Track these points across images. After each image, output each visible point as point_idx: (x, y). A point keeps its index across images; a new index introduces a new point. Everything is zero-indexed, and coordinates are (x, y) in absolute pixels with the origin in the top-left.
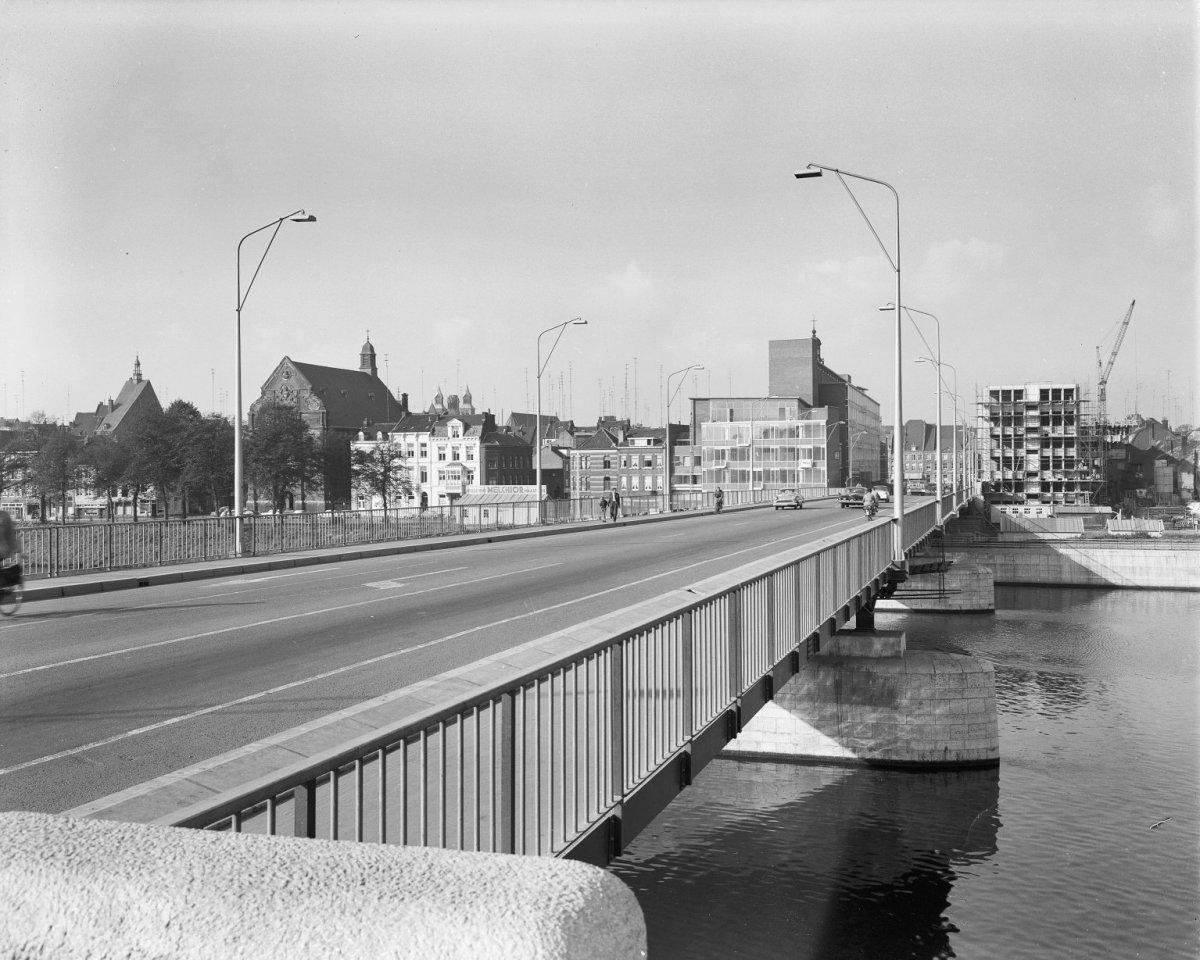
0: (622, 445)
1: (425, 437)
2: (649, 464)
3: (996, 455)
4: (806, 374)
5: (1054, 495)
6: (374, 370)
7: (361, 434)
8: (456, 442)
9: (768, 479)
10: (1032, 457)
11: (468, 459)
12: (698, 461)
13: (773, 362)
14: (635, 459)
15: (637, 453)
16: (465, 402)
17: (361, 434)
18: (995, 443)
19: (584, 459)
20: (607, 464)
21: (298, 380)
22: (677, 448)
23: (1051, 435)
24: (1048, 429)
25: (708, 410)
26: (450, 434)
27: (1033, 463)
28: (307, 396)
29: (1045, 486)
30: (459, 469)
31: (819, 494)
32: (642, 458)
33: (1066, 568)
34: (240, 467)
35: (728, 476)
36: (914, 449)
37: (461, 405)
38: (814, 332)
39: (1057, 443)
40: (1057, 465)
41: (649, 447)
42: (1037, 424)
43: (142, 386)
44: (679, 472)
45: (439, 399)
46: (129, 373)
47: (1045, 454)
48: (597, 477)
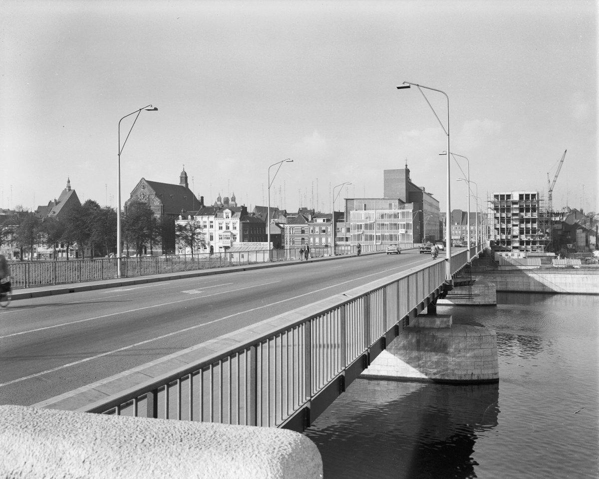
0: (310, 222)
1: (212, 218)
2: (324, 231)
3: (497, 227)
4: (403, 187)
5: (526, 247)
6: (187, 184)
7: (180, 216)
8: (228, 220)
9: (383, 239)
10: (515, 228)
11: (234, 229)
12: (348, 230)
13: (386, 181)
14: (317, 229)
15: (318, 226)
16: (232, 200)
17: (180, 216)
18: (496, 221)
19: (291, 229)
20: (303, 232)
21: (149, 190)
22: (338, 223)
23: (525, 217)
24: (523, 214)
25: (353, 204)
26: (225, 216)
27: (516, 231)
28: (153, 197)
29: (522, 242)
30: (229, 234)
31: (409, 246)
32: (320, 229)
33: (532, 284)
34: (120, 233)
35: (363, 238)
36: (456, 224)
37: (230, 202)
38: (406, 166)
39: (528, 221)
40: (528, 232)
41: (324, 223)
42: (517, 212)
43: (71, 193)
44: (339, 235)
45: (219, 199)
46: (64, 186)
47: (522, 227)
48: (298, 238)
